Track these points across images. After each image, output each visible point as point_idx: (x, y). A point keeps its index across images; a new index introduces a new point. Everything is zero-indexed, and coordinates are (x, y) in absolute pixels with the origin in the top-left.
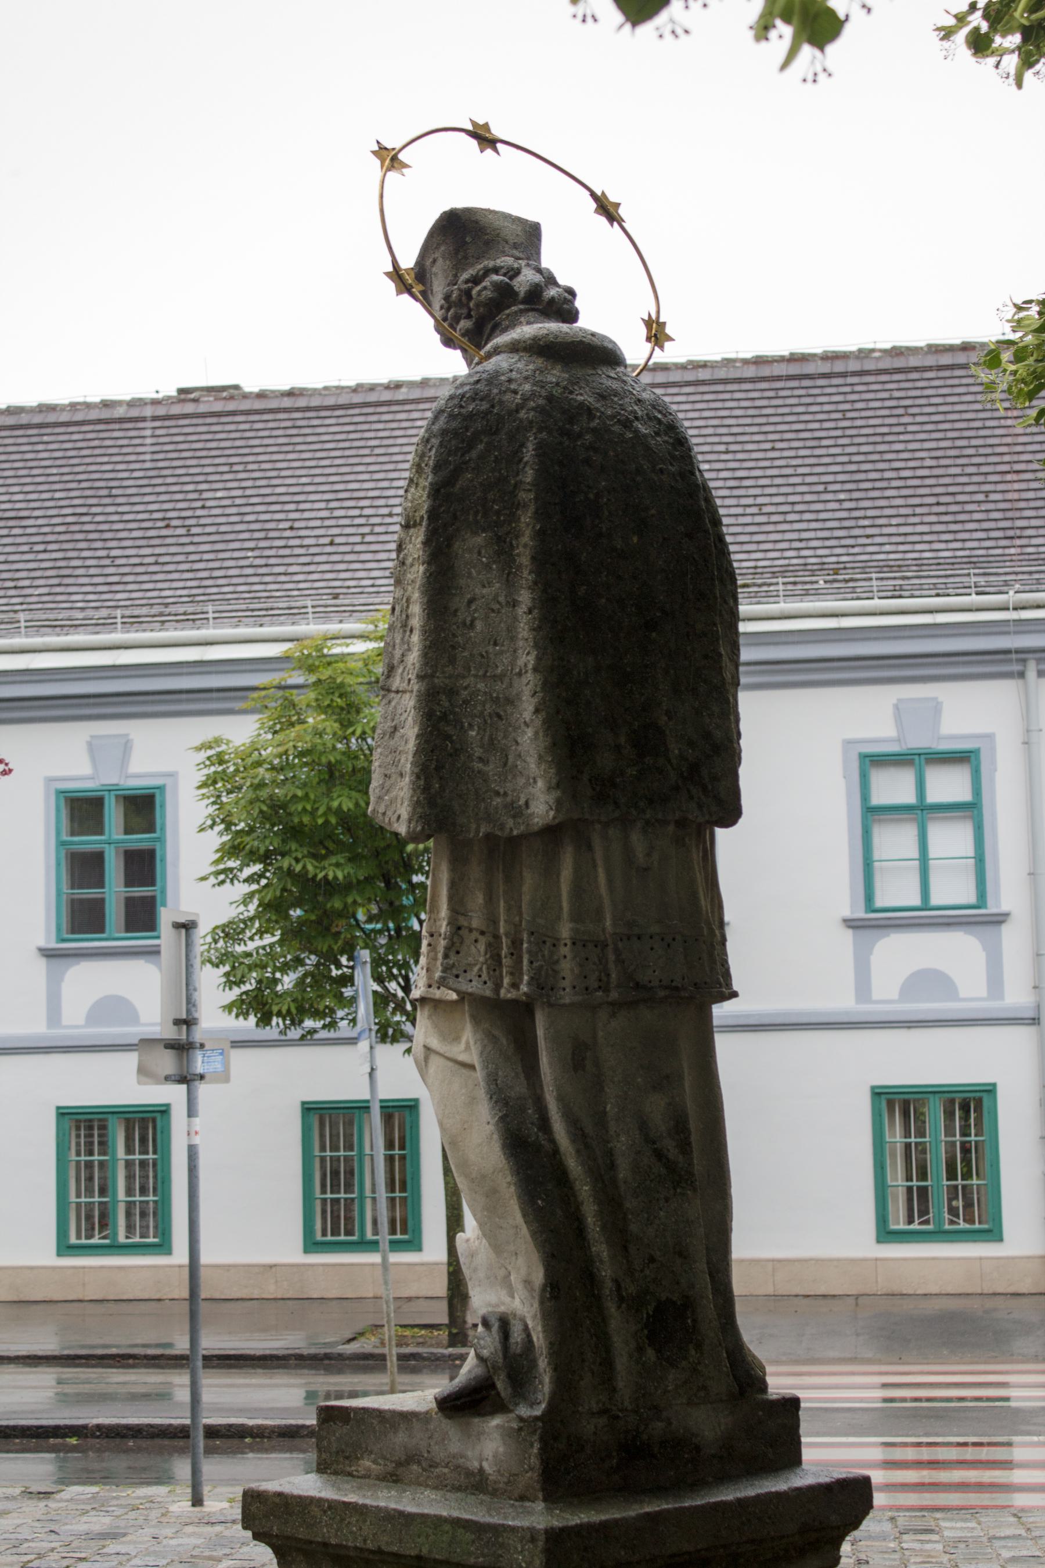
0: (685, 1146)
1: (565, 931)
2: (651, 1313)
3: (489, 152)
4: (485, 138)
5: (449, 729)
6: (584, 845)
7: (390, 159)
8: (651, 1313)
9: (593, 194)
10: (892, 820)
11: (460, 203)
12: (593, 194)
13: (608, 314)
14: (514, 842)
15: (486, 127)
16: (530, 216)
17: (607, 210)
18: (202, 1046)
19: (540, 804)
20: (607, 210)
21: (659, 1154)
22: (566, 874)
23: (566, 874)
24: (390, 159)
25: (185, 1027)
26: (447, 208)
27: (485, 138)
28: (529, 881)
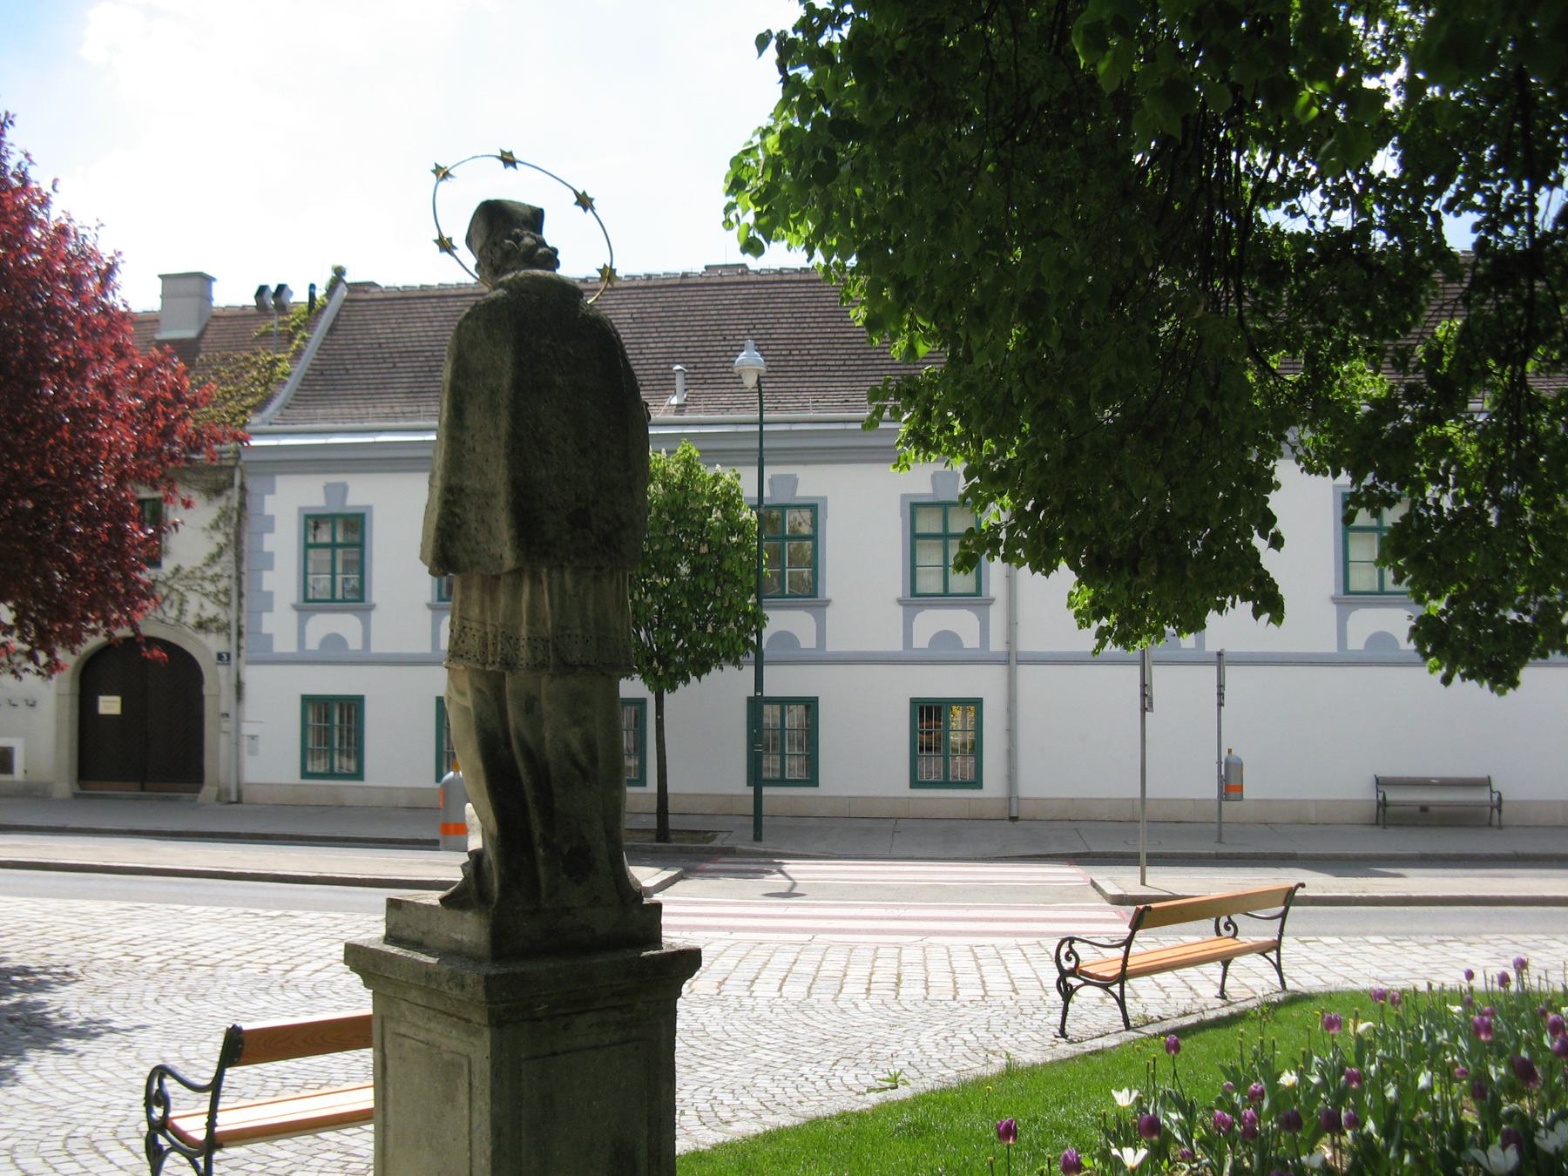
0: (593, 760)
1: (524, 632)
2: (26, 647)
3: (511, 168)
4: (508, 160)
5: (458, 510)
6: (536, 579)
7: (442, 173)
8: (26, 647)
9: (576, 193)
10: (116, 798)
11: (492, 197)
12: (576, 193)
13: (576, 264)
14: (497, 578)
15: (511, 154)
16: (538, 205)
17: (584, 202)
18: (762, 41)
19: (509, 561)
20: (584, 202)
21: (576, 764)
22: (526, 596)
23: (526, 596)
24: (442, 173)
25: (336, 770)
26: (484, 199)
27: (508, 160)
28: (503, 599)
